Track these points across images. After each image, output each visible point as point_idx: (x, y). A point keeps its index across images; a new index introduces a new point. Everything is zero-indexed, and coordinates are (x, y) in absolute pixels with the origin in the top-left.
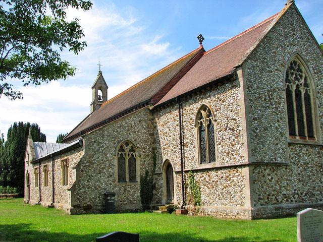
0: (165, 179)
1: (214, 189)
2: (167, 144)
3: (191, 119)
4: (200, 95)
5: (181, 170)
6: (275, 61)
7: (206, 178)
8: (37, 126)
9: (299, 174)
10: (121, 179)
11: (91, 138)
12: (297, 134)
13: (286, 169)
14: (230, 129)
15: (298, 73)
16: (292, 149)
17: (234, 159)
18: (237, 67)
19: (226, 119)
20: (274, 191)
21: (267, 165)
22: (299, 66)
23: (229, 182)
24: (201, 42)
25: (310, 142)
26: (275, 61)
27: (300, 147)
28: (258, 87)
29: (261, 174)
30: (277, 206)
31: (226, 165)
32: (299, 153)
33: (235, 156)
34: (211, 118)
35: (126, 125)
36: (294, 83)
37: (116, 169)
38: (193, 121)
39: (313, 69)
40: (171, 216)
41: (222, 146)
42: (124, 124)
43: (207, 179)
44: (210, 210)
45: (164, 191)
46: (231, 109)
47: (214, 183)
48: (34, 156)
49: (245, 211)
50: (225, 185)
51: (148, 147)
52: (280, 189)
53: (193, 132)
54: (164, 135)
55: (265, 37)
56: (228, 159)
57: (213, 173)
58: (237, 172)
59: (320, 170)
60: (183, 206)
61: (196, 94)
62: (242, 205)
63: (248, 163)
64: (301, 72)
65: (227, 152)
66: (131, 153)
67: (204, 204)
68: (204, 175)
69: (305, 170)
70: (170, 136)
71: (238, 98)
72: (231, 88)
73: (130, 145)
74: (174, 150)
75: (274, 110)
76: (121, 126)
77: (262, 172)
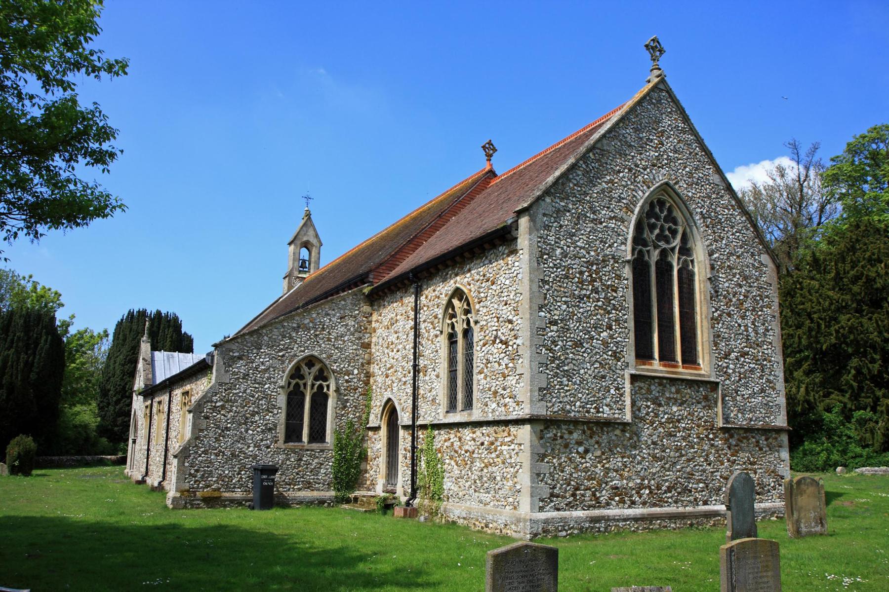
0: (384, 440)
1: (468, 466)
2: (392, 367)
3: (436, 317)
4: (453, 269)
5: (411, 423)
6: (611, 198)
7: (455, 444)
8: (176, 319)
9: (654, 443)
10: (293, 433)
11: (232, 351)
12: (656, 355)
13: (623, 431)
14: (501, 342)
15: (667, 226)
16: (641, 388)
17: (505, 405)
18: (520, 213)
19: (496, 319)
20: (590, 479)
21: (576, 422)
22: (670, 210)
23: (493, 455)
24: (489, 157)
25: (684, 372)
26: (611, 198)
27: (660, 384)
28: (565, 255)
29: (559, 441)
30: (596, 512)
31: (490, 417)
32: (657, 398)
33: (507, 400)
34: (469, 316)
35: (311, 325)
36: (656, 247)
37: (282, 417)
38: (439, 322)
39: (703, 217)
40: (386, 519)
41: (485, 378)
42: (307, 321)
43: (457, 444)
44: (457, 512)
45: (380, 466)
46: (505, 299)
47: (467, 454)
48: (148, 379)
49: (519, 520)
50: (486, 461)
51: (356, 372)
52: (605, 476)
53: (438, 345)
54: (387, 348)
55: (591, 149)
56: (494, 405)
57: (467, 433)
58: (509, 435)
59: (707, 436)
60: (410, 499)
61: (447, 266)
62: (515, 508)
63: (528, 417)
64: (675, 223)
65: (493, 389)
66: (318, 383)
67: (448, 499)
68: (452, 436)
69: (670, 435)
70: (398, 351)
71: (520, 276)
72: (508, 256)
73: (317, 367)
74: (404, 379)
75: (600, 304)
76: (299, 327)
77: (562, 437)
